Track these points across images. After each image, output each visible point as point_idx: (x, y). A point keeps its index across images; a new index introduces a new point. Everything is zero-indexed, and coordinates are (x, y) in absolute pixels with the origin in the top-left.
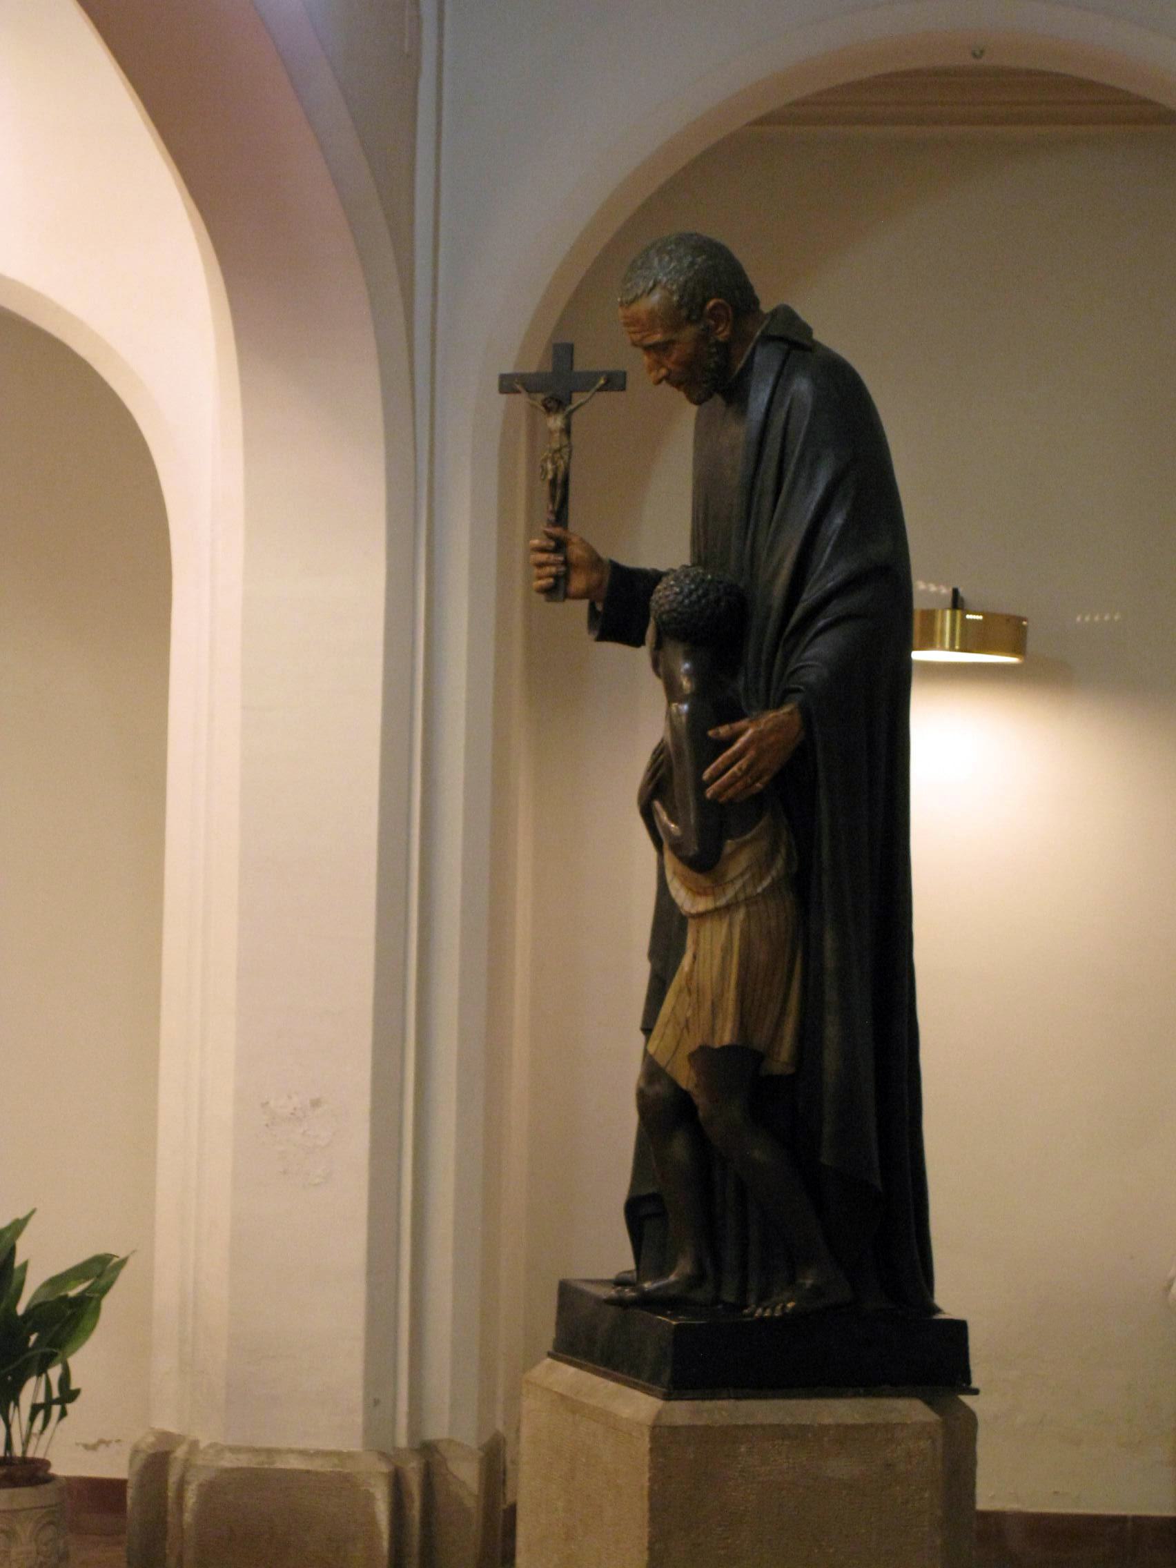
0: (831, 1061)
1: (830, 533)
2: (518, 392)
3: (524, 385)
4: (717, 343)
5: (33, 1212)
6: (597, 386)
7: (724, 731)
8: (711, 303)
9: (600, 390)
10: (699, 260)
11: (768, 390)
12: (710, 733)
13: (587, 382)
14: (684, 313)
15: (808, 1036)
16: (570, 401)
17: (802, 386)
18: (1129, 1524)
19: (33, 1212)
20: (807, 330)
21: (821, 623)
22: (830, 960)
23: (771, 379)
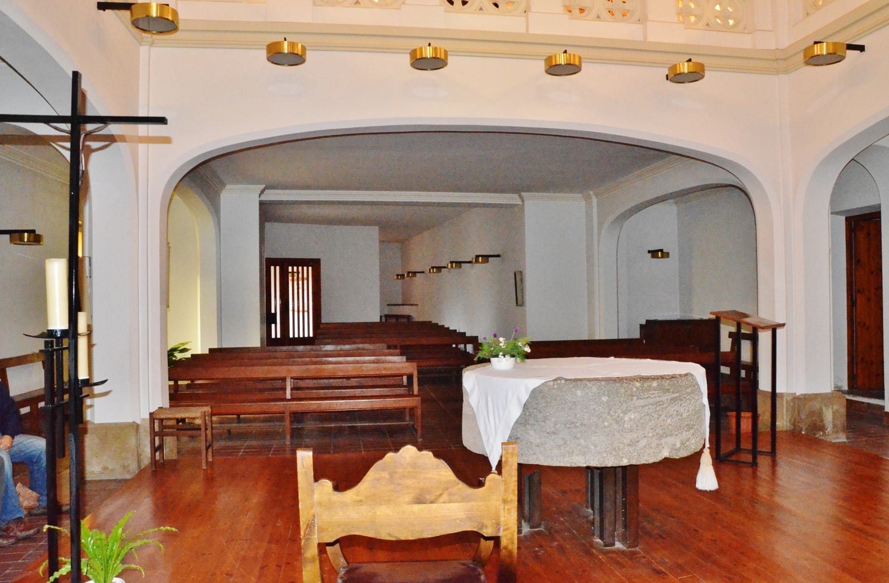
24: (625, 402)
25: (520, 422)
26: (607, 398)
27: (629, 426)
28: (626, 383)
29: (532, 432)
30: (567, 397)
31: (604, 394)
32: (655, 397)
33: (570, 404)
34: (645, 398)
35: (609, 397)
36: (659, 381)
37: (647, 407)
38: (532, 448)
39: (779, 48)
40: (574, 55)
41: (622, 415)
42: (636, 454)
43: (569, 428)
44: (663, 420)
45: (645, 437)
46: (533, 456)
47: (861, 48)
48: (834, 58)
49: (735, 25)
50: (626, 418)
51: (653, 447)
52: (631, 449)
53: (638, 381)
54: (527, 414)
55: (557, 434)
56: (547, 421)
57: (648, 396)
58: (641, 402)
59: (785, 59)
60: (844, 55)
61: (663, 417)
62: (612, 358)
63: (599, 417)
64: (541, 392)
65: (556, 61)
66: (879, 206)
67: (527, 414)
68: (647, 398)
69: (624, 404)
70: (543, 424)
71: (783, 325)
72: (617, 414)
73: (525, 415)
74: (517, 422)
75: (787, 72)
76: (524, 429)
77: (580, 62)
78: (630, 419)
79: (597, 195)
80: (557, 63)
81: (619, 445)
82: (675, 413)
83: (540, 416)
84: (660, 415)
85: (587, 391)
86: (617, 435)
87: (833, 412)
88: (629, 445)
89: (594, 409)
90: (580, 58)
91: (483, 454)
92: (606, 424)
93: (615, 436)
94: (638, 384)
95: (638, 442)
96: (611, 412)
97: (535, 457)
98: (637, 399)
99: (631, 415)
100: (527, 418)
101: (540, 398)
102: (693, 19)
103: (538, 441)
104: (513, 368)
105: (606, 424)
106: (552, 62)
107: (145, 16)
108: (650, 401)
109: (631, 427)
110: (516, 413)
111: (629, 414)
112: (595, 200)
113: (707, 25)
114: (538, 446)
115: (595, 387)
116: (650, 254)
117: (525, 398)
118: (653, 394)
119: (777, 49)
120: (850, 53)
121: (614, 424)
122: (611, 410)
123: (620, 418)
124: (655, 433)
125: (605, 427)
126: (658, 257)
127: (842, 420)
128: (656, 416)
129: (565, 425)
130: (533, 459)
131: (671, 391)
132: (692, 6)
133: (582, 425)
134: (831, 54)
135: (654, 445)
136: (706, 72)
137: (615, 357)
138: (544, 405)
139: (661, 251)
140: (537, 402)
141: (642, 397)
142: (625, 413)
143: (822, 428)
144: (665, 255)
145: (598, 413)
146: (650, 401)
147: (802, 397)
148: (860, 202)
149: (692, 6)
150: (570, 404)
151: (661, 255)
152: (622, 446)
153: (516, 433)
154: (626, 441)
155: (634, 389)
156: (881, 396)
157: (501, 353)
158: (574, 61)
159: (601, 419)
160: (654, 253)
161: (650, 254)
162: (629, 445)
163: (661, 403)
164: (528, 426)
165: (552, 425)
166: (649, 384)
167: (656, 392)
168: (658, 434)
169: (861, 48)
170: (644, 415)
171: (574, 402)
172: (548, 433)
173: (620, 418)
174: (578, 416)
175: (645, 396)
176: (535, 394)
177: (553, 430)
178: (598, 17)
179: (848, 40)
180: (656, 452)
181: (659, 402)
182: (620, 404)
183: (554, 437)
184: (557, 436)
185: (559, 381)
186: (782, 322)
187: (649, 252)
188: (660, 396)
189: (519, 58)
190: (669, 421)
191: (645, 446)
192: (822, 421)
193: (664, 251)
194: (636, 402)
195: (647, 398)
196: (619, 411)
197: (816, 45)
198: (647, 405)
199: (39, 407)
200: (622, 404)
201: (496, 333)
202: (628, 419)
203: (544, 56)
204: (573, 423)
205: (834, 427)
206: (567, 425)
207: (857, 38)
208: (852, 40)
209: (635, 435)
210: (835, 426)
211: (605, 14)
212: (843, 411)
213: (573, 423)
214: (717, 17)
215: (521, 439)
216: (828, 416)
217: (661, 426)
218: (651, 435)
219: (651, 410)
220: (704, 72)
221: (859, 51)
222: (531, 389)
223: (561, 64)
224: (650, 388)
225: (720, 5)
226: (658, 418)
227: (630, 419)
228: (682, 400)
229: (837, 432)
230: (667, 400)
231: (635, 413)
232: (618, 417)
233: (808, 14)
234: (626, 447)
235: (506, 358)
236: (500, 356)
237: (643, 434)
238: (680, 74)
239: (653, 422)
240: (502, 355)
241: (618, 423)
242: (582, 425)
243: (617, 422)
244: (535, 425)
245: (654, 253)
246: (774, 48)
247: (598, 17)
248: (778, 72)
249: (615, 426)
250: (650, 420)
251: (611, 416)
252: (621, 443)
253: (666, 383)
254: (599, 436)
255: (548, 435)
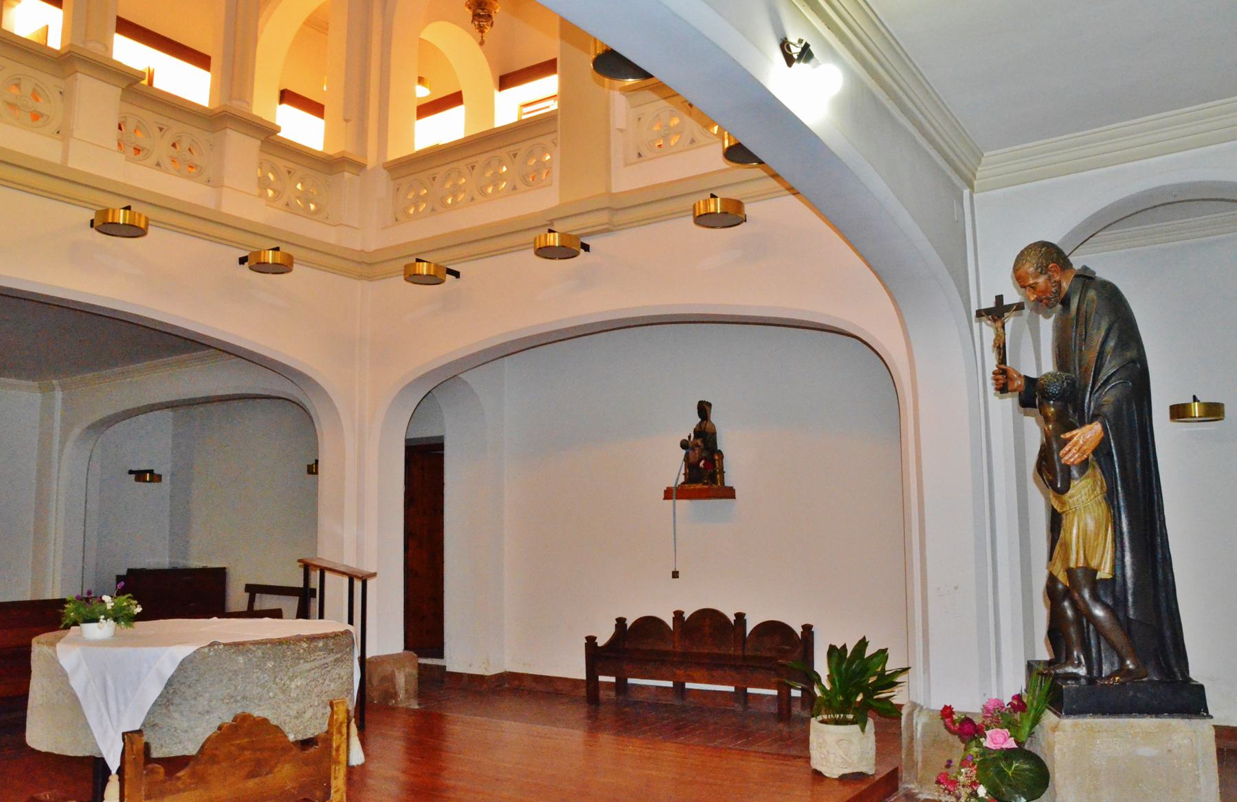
0: (1129, 572)
1: (1113, 392)
2: (984, 316)
3: (985, 313)
4: (1055, 282)
5: (704, 409)
6: (1013, 309)
7: (1068, 435)
8: (1050, 266)
9: (1015, 310)
10: (1043, 249)
11: (1078, 297)
12: (1062, 436)
13: (1009, 308)
14: (1039, 270)
15: (1118, 561)
16: (1004, 316)
17: (1092, 294)
18: (441, 452)
19: (704, 409)
20: (1094, 273)
21: (1097, 388)
22: (1166, 625)
23: (1079, 294)
24: (292, 666)
25: (159, 703)
26: (273, 663)
27: (295, 695)
28: (294, 645)
29: (176, 715)
30: (226, 665)
31: (269, 659)
32: (321, 659)
33: (230, 674)
34: (311, 661)
35: (275, 661)
36: (325, 640)
37: (313, 672)
38: (177, 735)
39: (366, 250)
40: (140, 215)
41: (288, 682)
42: (302, 727)
43: (227, 703)
44: (328, 685)
45: (311, 706)
46: (178, 745)
47: (456, 274)
48: (433, 280)
49: (317, 212)
50: (293, 686)
51: (319, 717)
52: (297, 723)
53: (304, 641)
54: (171, 691)
55: (212, 713)
56: (198, 698)
57: (314, 658)
58: (308, 666)
59: (370, 264)
60: (443, 279)
61: (327, 682)
62: (215, 619)
63: (263, 686)
64: (191, 662)
65: (113, 218)
66: (442, 438)
67: (171, 691)
68: (314, 660)
69: (291, 669)
70: (193, 702)
71: (374, 575)
72: (283, 682)
73: (168, 692)
74: (155, 704)
75: (370, 278)
76: (164, 711)
77: (147, 225)
78: (297, 687)
79: (63, 388)
80: (115, 221)
81: (285, 718)
82: (337, 677)
83: (190, 692)
84: (325, 680)
85: (250, 656)
86: (283, 707)
87: (405, 675)
88: (296, 718)
89: (258, 678)
90: (147, 219)
91: (92, 755)
92: (271, 694)
93: (280, 708)
94: (305, 645)
95: (304, 712)
96: (277, 679)
97: (181, 746)
98: (304, 662)
99: (297, 681)
100: (170, 697)
101: (191, 669)
102: (270, 193)
103: (185, 725)
104: (113, 636)
105: (271, 694)
106: (107, 219)
107: (101, 223)
108: (317, 664)
109: (297, 695)
110: (154, 691)
111: (296, 680)
112: (59, 395)
113: (287, 205)
114: (186, 731)
115: (259, 651)
116: (133, 476)
117: (169, 670)
118: (318, 655)
119: (362, 251)
120: (449, 277)
121: (280, 694)
122: (276, 677)
123: (287, 686)
124: (320, 701)
125: (270, 698)
126: (145, 481)
127: (414, 685)
128: (321, 681)
129: (222, 700)
130: (178, 749)
131: (335, 651)
132: (271, 176)
133: (244, 698)
134: (431, 275)
135: (319, 715)
136: (294, 265)
137: (219, 617)
138: (195, 677)
139: (151, 472)
140: (186, 675)
141: (309, 660)
142: (291, 679)
143: (395, 695)
144: (156, 478)
145: (263, 681)
146: (317, 664)
147: (372, 660)
148: (426, 431)
149: (271, 176)
150: (230, 674)
151: (150, 478)
152: (288, 719)
153: (152, 719)
154: (293, 713)
155: (302, 651)
156: (440, 655)
157: (102, 617)
158: (139, 222)
159: (266, 689)
160: (140, 475)
161: (133, 476)
162: (296, 718)
163: (326, 666)
164: (171, 708)
165: (206, 703)
166: (316, 644)
167: (321, 653)
168: (323, 701)
169: (456, 274)
170: (311, 681)
171: (235, 671)
172: (200, 713)
173: (287, 686)
174: (239, 688)
175: (312, 659)
176: (183, 666)
177: (207, 708)
178: (158, 165)
179: (421, 253)
180: (322, 722)
181: (324, 665)
182: (286, 669)
183: (207, 717)
184: (212, 715)
185: (216, 647)
186: (372, 571)
187: (131, 472)
188: (325, 658)
189: (19, 190)
190: (332, 686)
191: (311, 718)
192: (394, 687)
193: (155, 472)
194: (305, 666)
195: (314, 660)
196: (286, 678)
197: (417, 263)
198: (313, 669)
199: (1098, 577)
200: (289, 669)
201: (93, 591)
202: (294, 687)
203: (99, 206)
204: (232, 697)
205: (406, 693)
206: (225, 701)
207: (452, 262)
208: (447, 263)
209: (301, 705)
210: (407, 691)
211: (166, 162)
212: (415, 672)
213: (232, 697)
214: (298, 198)
215: (160, 726)
216: (401, 680)
217: (325, 692)
218: (316, 703)
219: (317, 675)
220: (292, 266)
221: (455, 277)
222: (180, 661)
223: (119, 224)
224: (316, 649)
225: (301, 183)
226: (323, 683)
227: (297, 687)
228: (342, 661)
229: (408, 698)
230: (331, 662)
231: (301, 679)
232: (284, 685)
233: (397, 220)
234: (292, 720)
235: (108, 622)
236: (101, 620)
237: (309, 703)
238: (264, 263)
239: (319, 688)
240: (104, 619)
241: (284, 693)
242: (244, 698)
243: (284, 692)
244: (181, 704)
245: (140, 475)
246: (359, 249)
247: (158, 165)
248: (361, 277)
249: (281, 696)
250: (316, 686)
251: (277, 684)
252: (287, 716)
253: (331, 642)
254: (263, 710)
255: (200, 715)
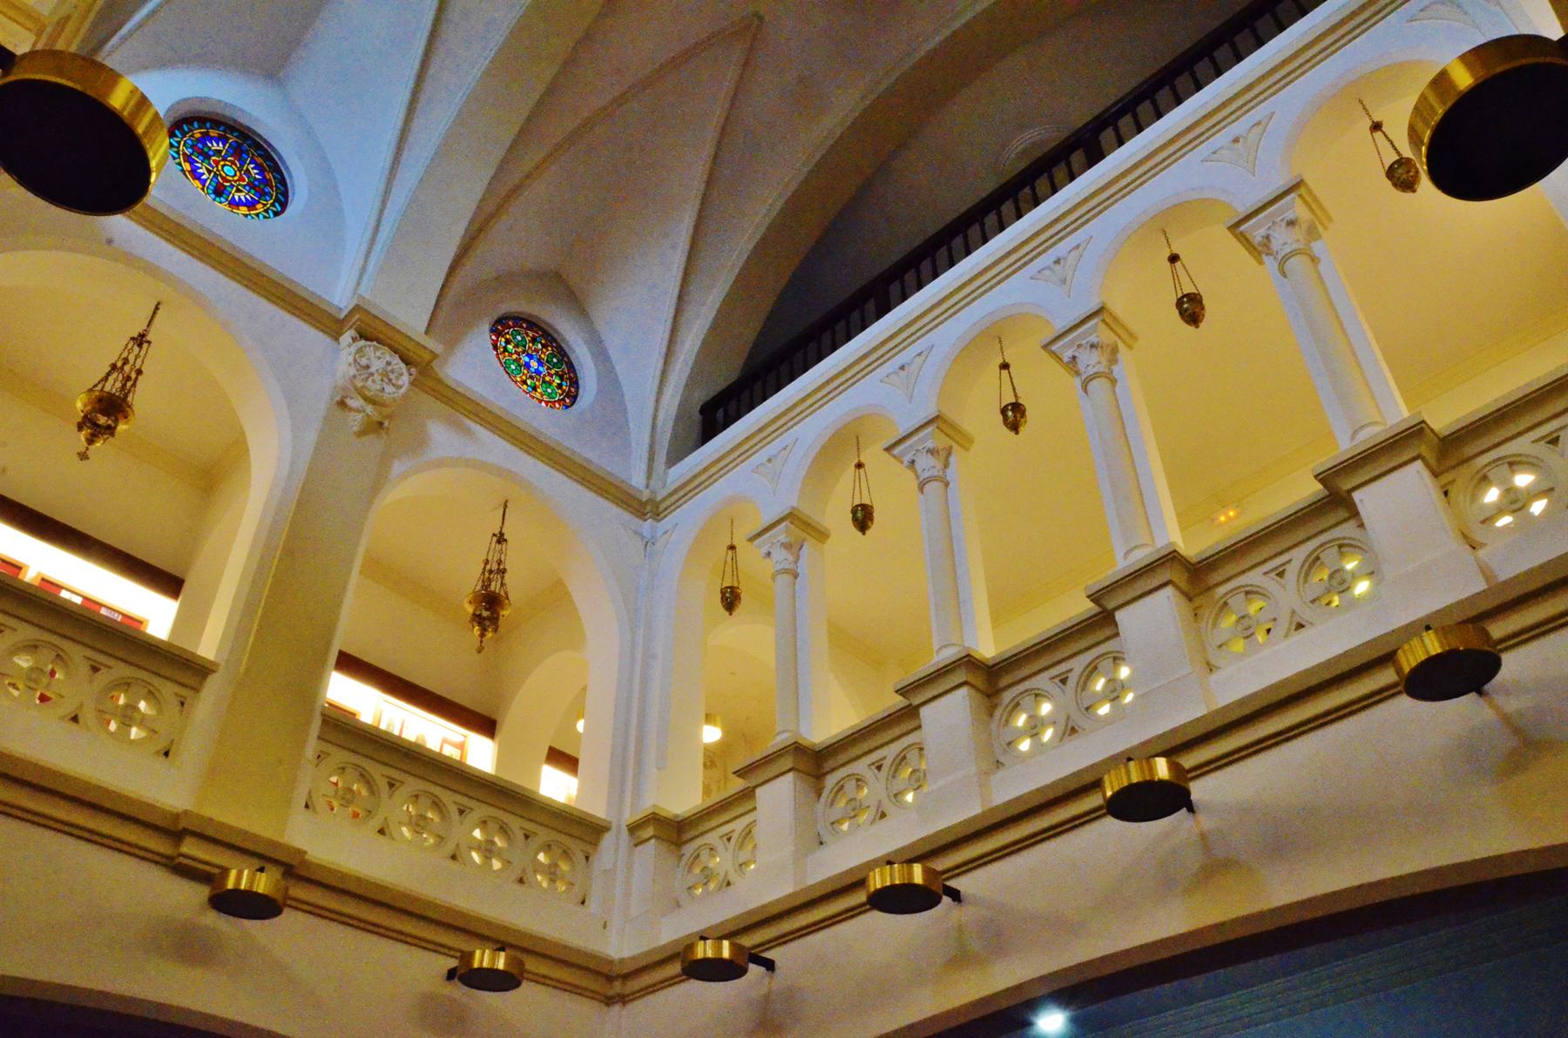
47: (770, 965)
